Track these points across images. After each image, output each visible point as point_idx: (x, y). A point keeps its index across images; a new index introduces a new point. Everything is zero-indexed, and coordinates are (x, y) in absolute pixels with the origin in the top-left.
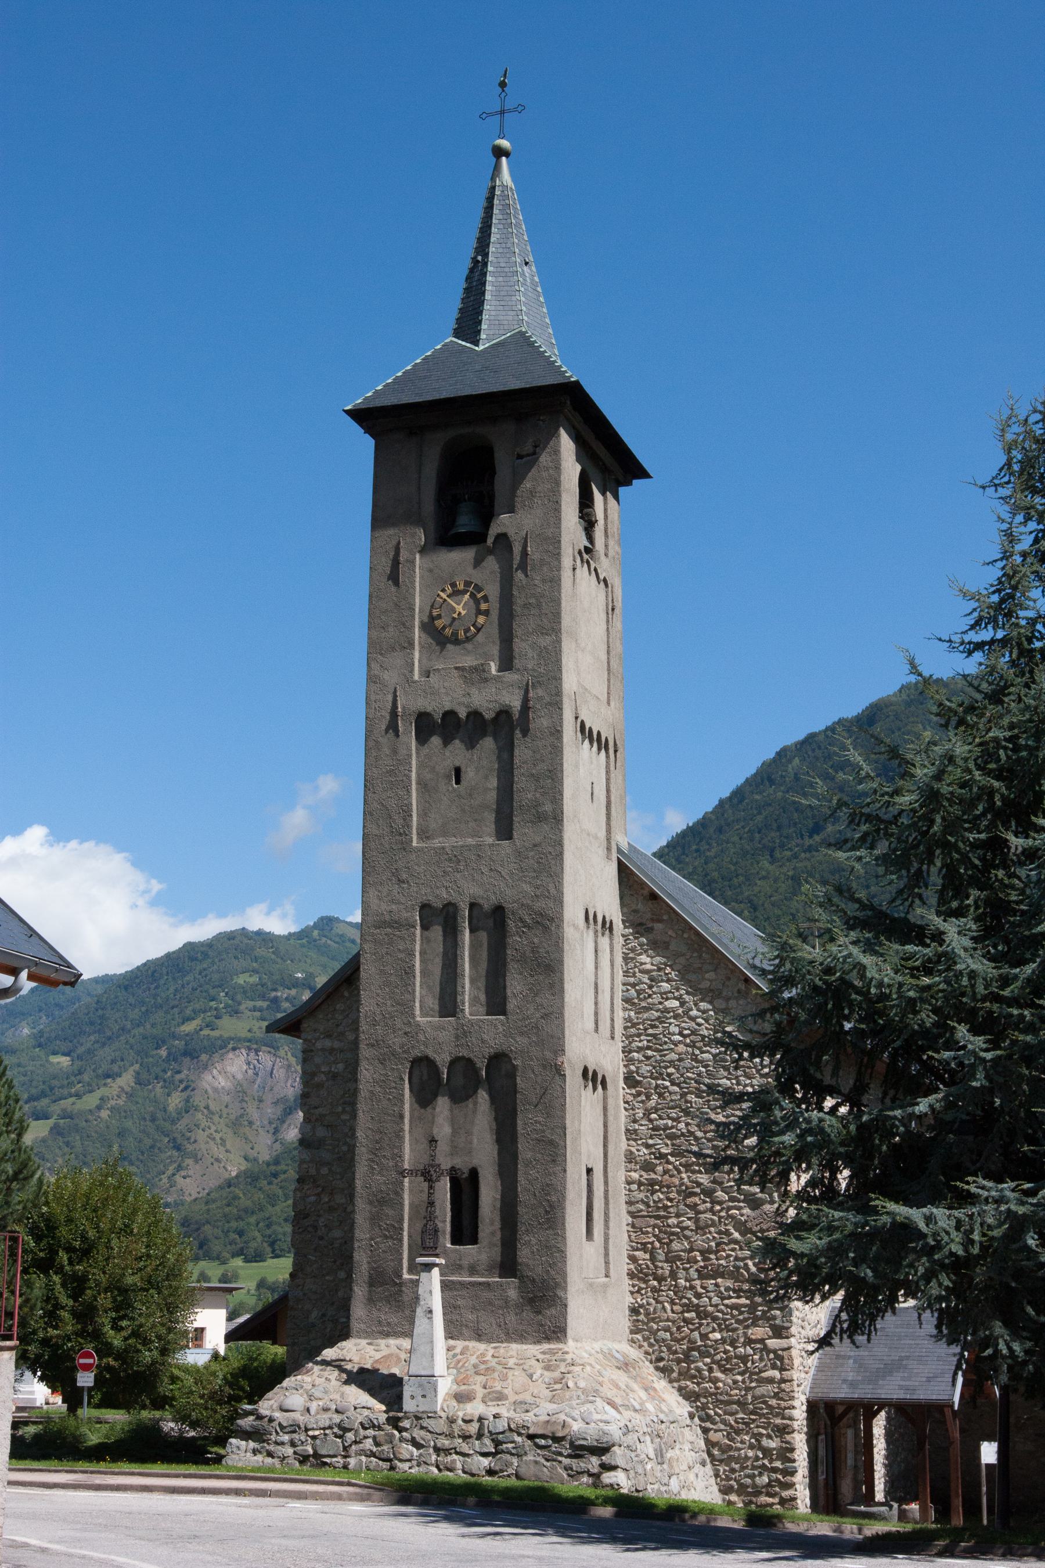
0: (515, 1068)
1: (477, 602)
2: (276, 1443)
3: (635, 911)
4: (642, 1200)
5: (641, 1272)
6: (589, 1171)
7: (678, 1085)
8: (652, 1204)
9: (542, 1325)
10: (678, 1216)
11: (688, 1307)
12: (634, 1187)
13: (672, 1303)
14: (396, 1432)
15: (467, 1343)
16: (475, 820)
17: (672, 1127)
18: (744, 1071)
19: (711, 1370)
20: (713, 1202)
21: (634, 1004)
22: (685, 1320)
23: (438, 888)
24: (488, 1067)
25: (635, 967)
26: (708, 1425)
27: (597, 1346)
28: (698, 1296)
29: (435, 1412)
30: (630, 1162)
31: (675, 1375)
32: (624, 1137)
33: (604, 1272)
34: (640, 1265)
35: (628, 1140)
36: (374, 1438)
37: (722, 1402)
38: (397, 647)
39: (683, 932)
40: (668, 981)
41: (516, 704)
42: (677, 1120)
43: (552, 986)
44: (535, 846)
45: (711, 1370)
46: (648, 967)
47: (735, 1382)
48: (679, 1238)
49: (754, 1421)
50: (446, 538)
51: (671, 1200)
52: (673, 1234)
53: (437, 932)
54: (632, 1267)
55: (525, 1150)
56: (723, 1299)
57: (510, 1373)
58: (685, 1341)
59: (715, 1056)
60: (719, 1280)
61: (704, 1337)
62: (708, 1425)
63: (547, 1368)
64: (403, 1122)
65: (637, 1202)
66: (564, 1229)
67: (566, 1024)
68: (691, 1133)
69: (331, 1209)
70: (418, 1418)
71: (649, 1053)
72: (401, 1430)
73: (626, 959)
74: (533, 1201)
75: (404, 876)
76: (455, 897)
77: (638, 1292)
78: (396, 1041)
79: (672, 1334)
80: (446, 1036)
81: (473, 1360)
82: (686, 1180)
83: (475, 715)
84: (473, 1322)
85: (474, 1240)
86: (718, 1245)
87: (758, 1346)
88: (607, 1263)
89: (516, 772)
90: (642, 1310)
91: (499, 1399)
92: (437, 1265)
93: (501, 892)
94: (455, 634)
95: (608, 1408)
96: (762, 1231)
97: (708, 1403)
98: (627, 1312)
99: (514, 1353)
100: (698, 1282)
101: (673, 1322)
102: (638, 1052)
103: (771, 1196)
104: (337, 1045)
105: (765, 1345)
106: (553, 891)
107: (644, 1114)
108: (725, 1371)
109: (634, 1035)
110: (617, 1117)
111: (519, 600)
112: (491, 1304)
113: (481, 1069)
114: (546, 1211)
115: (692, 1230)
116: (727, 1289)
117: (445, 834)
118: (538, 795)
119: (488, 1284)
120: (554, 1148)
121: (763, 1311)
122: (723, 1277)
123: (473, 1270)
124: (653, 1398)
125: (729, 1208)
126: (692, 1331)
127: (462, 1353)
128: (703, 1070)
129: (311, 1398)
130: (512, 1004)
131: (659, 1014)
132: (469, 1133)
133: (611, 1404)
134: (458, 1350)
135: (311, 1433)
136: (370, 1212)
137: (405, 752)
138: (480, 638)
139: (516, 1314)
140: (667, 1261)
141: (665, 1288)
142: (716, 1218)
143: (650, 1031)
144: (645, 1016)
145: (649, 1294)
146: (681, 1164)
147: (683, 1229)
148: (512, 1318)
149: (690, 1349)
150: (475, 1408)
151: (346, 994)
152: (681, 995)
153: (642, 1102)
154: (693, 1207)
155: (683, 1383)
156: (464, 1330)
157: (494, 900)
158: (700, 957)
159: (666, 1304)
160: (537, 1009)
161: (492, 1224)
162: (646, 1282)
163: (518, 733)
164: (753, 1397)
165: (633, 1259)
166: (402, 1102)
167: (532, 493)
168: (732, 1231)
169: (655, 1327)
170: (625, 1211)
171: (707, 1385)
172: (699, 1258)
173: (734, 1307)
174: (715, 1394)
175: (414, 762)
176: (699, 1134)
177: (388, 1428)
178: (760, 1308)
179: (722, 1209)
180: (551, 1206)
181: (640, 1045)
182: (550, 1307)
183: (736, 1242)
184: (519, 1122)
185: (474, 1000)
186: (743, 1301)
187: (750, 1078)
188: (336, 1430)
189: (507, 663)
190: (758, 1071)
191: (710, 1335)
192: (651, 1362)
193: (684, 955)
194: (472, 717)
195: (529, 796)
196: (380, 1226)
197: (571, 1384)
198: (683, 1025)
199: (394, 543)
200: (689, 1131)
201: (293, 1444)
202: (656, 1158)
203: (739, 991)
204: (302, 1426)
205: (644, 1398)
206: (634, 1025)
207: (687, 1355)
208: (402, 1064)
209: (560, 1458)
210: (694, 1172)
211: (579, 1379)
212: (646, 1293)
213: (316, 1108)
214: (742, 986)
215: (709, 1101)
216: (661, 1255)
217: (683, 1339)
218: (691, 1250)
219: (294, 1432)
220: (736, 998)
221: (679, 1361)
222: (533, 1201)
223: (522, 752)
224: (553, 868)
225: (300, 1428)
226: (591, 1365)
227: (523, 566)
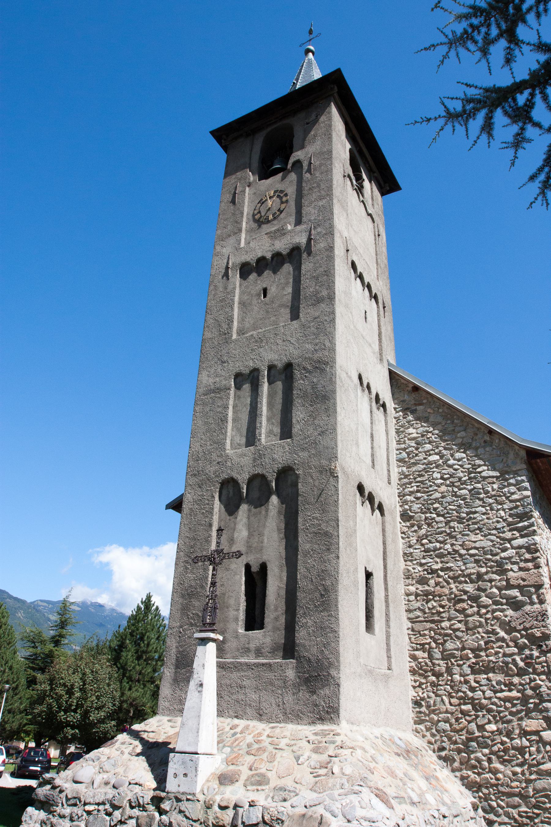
0: (297, 476)
3: (403, 401)
4: (419, 608)
5: (421, 668)
6: (369, 575)
7: (443, 516)
8: (427, 610)
9: (316, 705)
10: (449, 619)
11: (464, 700)
12: (412, 598)
13: (450, 696)
14: (157, 814)
15: (249, 722)
17: (440, 548)
18: (496, 500)
19: (490, 761)
20: (479, 606)
21: (405, 462)
22: (462, 712)
24: (277, 480)
25: (405, 437)
26: (492, 817)
27: (377, 732)
28: (473, 689)
29: (194, 794)
30: (408, 578)
31: (456, 764)
32: (402, 559)
33: (386, 665)
34: (420, 663)
35: (405, 561)
37: (504, 794)
39: (439, 409)
40: (430, 443)
42: (444, 542)
43: (327, 410)
45: (490, 761)
46: (415, 435)
47: (515, 774)
48: (452, 638)
49: (538, 815)
51: (443, 607)
52: (447, 635)
53: (247, 387)
54: (413, 664)
55: (304, 542)
56: (495, 692)
57: (279, 753)
58: (464, 732)
59: (470, 491)
60: (491, 675)
61: (481, 728)
62: (492, 817)
63: (316, 751)
64: (211, 530)
65: (415, 610)
66: (337, 610)
67: (339, 438)
68: (456, 552)
70: (178, 800)
71: (419, 495)
72: (162, 812)
73: (398, 432)
74: (311, 587)
76: (258, 364)
77: (419, 686)
78: (211, 469)
79: (451, 725)
80: (247, 461)
81: (249, 739)
82: (454, 590)
83: (277, 255)
84: (255, 701)
85: (261, 626)
86: (486, 643)
87: (534, 737)
88: (389, 657)
89: (302, 278)
90: (423, 703)
91: (260, 783)
92: (214, 640)
95: (376, 801)
96: (525, 629)
97: (489, 794)
98: (411, 705)
99: (288, 734)
100: (471, 678)
101: (452, 713)
102: (410, 495)
103: (530, 598)
105: (540, 737)
106: (328, 344)
107: (417, 541)
108: (503, 762)
109: (407, 483)
110: (394, 541)
112: (272, 684)
113: (271, 481)
114: (322, 595)
115: (463, 631)
116: (499, 683)
117: (255, 329)
118: (317, 288)
119: (270, 665)
120: (328, 540)
121: (535, 703)
122: (494, 672)
123: (259, 653)
124: (435, 788)
125: (494, 611)
126: (469, 722)
127: (241, 733)
128: (462, 502)
129: (102, 770)
130: (296, 429)
131: (424, 466)
132: (261, 534)
133: (381, 796)
134: (238, 730)
135: (88, 808)
136: (182, 604)
139: (293, 694)
140: (443, 659)
141: (443, 683)
142: (483, 620)
143: (419, 479)
144: (414, 469)
145: (429, 688)
146: (449, 577)
147: (455, 630)
148: (289, 698)
149: (469, 740)
150: (235, 793)
152: (440, 451)
153: (415, 531)
154: (462, 611)
155: (465, 772)
156: (248, 710)
157: (285, 360)
158: (453, 422)
159: (444, 697)
160: (315, 429)
162: (426, 677)
163: (305, 255)
164: (534, 789)
165: (414, 658)
166: (212, 514)
167: (315, 136)
168: (498, 630)
169: (436, 718)
170: (405, 618)
171: (487, 776)
172: (471, 656)
173: (506, 700)
174: (496, 785)
176: (463, 552)
177: (151, 808)
178: (531, 701)
179: (488, 612)
180: (325, 590)
181: (411, 490)
182: (323, 686)
183: (503, 640)
184: (300, 520)
185: (270, 433)
186: (514, 694)
187: (501, 504)
188: (108, 806)
189: (298, 222)
190: (507, 498)
191: (487, 727)
192: (434, 751)
193: (440, 423)
196: (188, 615)
197: (336, 770)
198: (443, 471)
199: (234, 186)
200: (454, 550)
202: (428, 573)
203: (485, 442)
204: (83, 800)
205: (424, 788)
206: (406, 476)
207: (466, 744)
210: (461, 582)
211: (347, 765)
212: (426, 687)
214: (487, 438)
215: (469, 525)
216: (437, 654)
217: (462, 730)
218: (463, 649)
219: (75, 805)
220: (484, 447)
221: (459, 751)
222: (311, 587)
225: (80, 801)
226: (363, 749)
227: (309, 171)
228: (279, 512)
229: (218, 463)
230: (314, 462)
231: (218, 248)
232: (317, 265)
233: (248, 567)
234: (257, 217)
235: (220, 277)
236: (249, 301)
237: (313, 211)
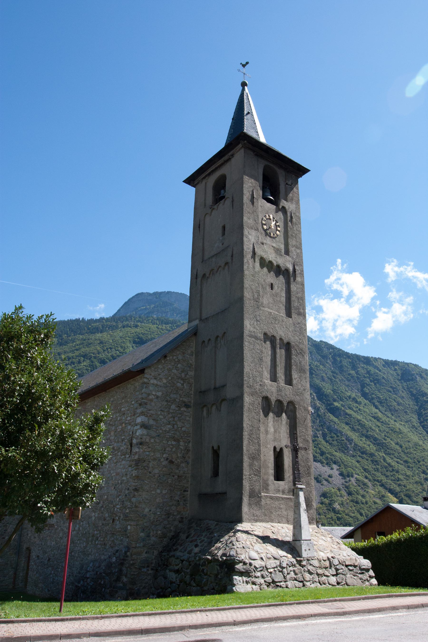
0: (295, 408)
2: (256, 577)
36: (294, 571)
44: (299, 323)
69: (154, 459)
70: (308, 560)
72: (303, 566)
80: (274, 389)
83: (278, 266)
84: (286, 515)
104: (159, 383)
111: (290, 233)
123: (283, 492)
130: (294, 382)
135: (269, 570)
136: (249, 462)
151: (163, 362)
161: (289, 473)
163: (292, 279)
180: (309, 467)
188: (279, 568)
196: (253, 469)
199: (252, 189)
201: (263, 577)
208: (259, 398)
209: (358, 575)
213: (150, 410)
228: (286, 423)
229: (260, 385)
230: (302, 403)
233: (275, 448)
235: (250, 256)
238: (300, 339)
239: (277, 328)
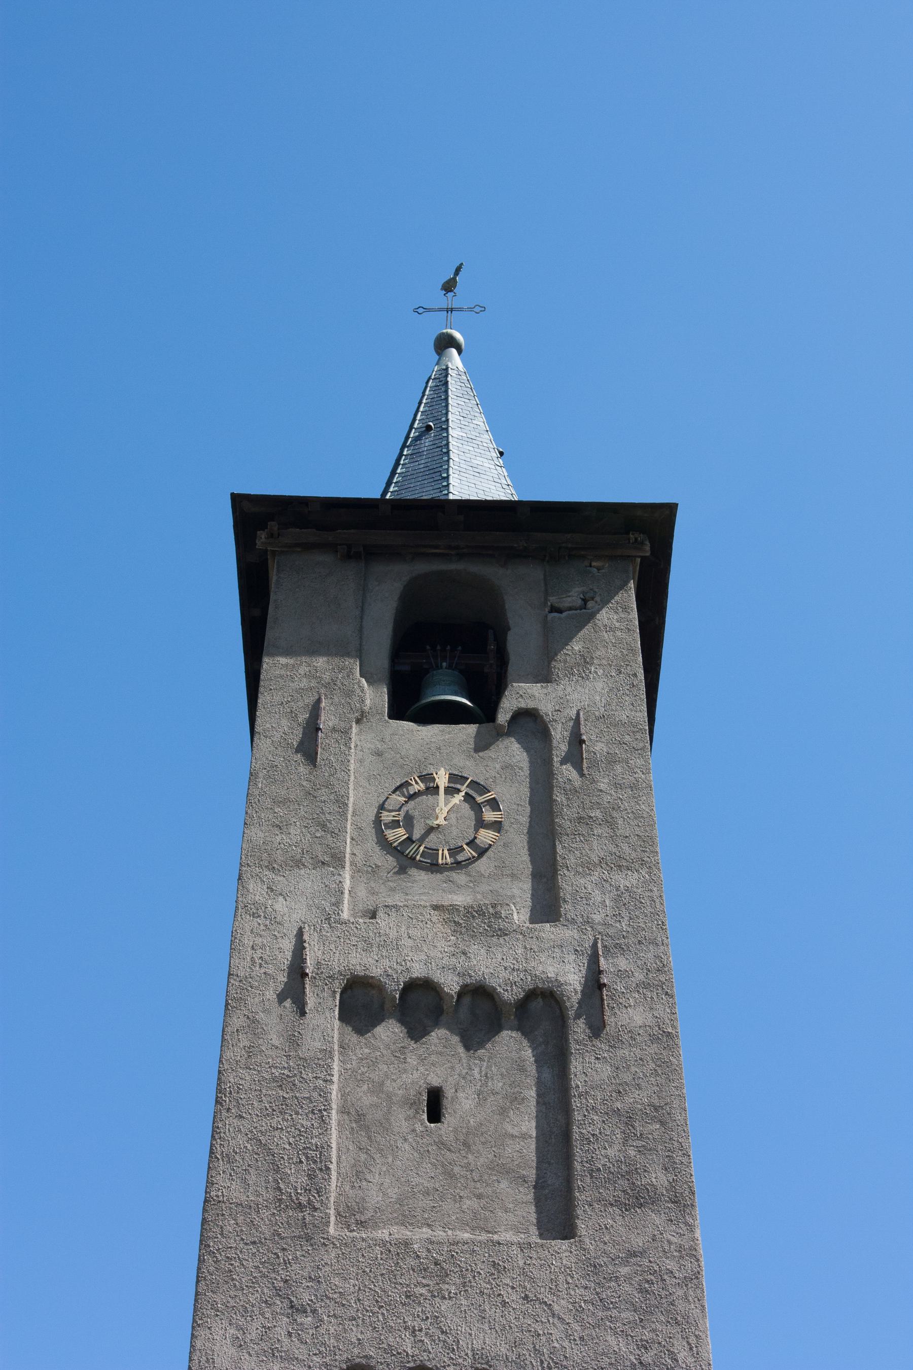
1: (477, 808)
16: (479, 1197)
23: (391, 1329)
38: (307, 860)
41: (571, 978)
44: (634, 1254)
50: (407, 704)
75: (306, 1297)
83: (478, 993)
89: (576, 1103)
93: (553, 1351)
94: (432, 853)
111: (567, 812)
118: (632, 1153)
137: (318, 1045)
138: (484, 865)
163: (579, 1029)
167: (586, 661)
175: (336, 1066)
189: (547, 907)
194: (467, 1000)
195: (611, 1152)
199: (310, 700)
223: (588, 1068)
224: (681, 1306)
227: (575, 756)
231: (256, 891)
232: (627, 1077)
234: (398, 835)
235: (271, 995)
236: (379, 1115)
237: (597, 896)
238: (645, 1346)
239: (452, 1321)
